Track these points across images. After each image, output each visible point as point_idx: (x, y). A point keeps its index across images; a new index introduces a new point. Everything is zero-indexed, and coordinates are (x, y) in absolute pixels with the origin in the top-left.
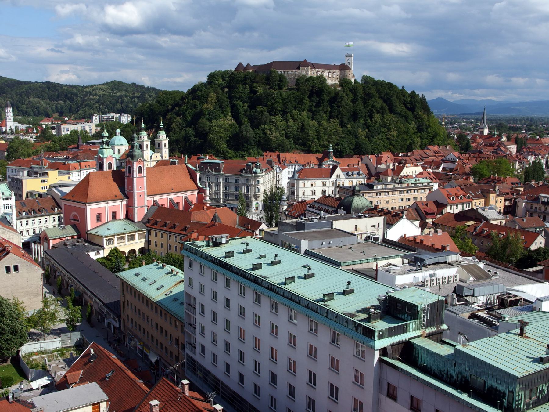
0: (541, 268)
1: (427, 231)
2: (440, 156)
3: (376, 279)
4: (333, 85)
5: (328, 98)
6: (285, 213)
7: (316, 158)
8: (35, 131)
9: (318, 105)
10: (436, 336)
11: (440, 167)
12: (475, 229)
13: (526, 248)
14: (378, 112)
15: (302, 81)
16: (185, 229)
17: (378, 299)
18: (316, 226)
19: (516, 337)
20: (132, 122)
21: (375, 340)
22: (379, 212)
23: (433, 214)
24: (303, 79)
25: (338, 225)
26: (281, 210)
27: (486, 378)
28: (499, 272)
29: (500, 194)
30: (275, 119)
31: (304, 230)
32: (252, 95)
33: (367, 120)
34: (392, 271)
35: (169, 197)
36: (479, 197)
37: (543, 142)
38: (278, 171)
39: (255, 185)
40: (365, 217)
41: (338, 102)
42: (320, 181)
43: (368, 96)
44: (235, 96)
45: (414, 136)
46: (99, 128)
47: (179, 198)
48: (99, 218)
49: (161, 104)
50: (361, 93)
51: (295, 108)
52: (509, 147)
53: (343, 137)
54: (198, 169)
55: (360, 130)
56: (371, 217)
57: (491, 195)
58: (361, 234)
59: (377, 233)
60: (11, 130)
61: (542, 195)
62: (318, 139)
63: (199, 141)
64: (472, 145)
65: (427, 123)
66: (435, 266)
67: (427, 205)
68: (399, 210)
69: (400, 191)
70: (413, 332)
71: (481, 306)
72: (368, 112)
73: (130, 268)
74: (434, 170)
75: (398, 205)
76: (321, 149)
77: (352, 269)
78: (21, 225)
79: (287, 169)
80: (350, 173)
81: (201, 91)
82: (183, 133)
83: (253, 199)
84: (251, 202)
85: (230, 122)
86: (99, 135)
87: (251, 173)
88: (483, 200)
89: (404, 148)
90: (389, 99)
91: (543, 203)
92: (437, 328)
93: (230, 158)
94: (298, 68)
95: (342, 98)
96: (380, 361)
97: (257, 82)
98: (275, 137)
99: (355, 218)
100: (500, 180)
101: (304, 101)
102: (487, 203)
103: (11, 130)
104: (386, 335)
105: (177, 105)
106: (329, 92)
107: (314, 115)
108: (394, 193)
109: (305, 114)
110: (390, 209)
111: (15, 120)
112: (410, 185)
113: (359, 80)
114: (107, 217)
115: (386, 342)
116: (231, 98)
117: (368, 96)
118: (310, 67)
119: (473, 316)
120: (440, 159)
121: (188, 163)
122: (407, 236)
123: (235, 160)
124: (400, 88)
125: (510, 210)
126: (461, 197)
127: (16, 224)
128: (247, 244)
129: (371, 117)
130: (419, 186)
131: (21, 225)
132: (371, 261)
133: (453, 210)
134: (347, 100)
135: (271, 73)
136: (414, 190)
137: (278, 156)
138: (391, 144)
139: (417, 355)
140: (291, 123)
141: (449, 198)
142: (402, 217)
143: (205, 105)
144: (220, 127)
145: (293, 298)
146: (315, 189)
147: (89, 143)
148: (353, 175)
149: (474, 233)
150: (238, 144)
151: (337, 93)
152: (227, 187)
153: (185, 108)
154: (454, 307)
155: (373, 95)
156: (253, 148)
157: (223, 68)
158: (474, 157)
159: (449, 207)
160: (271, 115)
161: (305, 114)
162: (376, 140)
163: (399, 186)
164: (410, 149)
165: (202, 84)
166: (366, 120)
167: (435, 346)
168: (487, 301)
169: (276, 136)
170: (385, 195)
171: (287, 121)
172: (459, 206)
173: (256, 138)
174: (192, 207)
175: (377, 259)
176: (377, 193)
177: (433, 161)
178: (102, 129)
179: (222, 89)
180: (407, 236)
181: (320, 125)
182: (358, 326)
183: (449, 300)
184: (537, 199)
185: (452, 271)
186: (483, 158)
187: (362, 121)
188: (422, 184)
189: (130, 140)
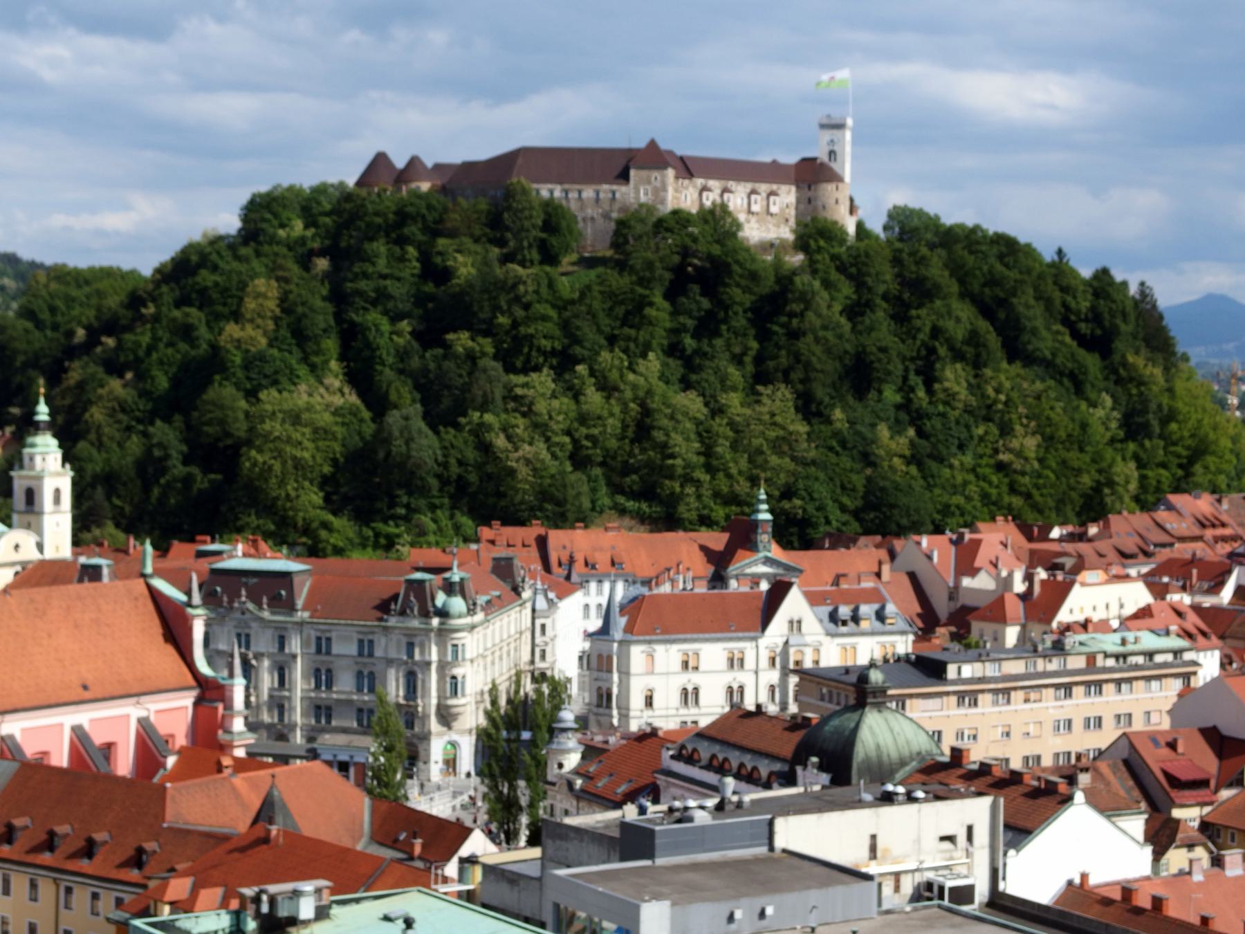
1: (1176, 858)
2: (1224, 539)
5: (748, 300)
6: (570, 785)
7: (704, 549)
9: (707, 327)
15: (639, 228)
16: (138, 859)
18: (703, 838)
23: (1202, 784)
24: (642, 221)
25: (795, 833)
26: (552, 772)
30: (526, 385)
32: (429, 288)
33: (912, 390)
38: (541, 603)
39: (443, 666)
40: (910, 799)
41: (792, 315)
43: (914, 291)
44: (360, 293)
45: (1109, 453)
47: (116, 723)
49: (39, 325)
50: (885, 278)
51: (612, 340)
53: (814, 463)
54: (197, 598)
55: (883, 431)
56: (938, 798)
58: (897, 875)
59: (964, 870)
62: (709, 468)
63: (202, 481)
65: (1165, 400)
67: (1172, 745)
69: (1057, 687)
72: (919, 357)
76: (720, 513)
80: (845, 611)
81: (215, 268)
82: (135, 445)
83: (434, 725)
84: (426, 737)
85: (338, 401)
87: (425, 615)
89: (1069, 507)
90: (1003, 303)
93: (338, 551)
94: (624, 177)
95: (806, 300)
97: (452, 234)
98: (528, 462)
105: (111, 326)
106: (754, 276)
107: (689, 369)
108: (1033, 696)
110: (1016, 765)
112: (1100, 661)
113: (876, 225)
116: (339, 298)
118: (670, 173)
121: (158, 573)
122: (1093, 881)
123: (356, 555)
124: (1048, 255)
129: (930, 380)
130: (1137, 667)
134: (829, 306)
135: (509, 194)
136: (1118, 682)
137: (542, 542)
138: (1013, 490)
140: (594, 398)
142: (1067, 800)
143: (232, 330)
144: (295, 418)
148: (856, 619)
150: (370, 491)
151: (785, 280)
152: (322, 676)
153: (146, 339)
155: (937, 287)
156: (433, 508)
157: (307, 176)
160: (510, 369)
164: (1093, 508)
165: (216, 241)
169: (527, 456)
170: (996, 703)
171: (576, 395)
173: (445, 465)
174: (171, 761)
177: (1194, 561)
179: (305, 261)
180: (1093, 881)
181: (717, 411)
188: (1150, 655)
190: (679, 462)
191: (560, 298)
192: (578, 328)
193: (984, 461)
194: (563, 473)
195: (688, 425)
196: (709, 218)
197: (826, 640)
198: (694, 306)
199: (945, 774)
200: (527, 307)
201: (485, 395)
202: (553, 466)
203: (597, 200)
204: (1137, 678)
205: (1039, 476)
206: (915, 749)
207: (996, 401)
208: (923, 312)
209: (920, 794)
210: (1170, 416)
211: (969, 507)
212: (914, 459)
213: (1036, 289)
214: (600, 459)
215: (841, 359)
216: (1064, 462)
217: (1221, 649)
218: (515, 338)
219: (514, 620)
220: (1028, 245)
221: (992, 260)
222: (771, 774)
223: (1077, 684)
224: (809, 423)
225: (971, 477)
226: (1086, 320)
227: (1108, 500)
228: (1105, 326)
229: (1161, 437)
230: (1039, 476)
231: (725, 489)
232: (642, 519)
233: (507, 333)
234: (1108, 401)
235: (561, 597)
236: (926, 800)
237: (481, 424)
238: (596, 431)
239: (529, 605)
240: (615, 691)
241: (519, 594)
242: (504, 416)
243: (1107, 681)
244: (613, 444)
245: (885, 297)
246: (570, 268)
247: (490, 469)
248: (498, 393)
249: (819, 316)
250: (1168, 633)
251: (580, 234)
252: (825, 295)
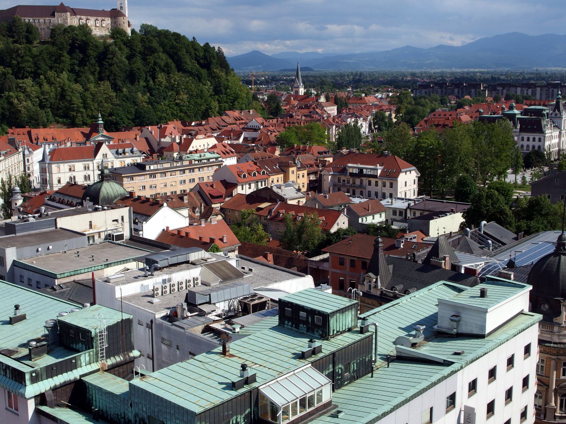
0: (326, 256)
2: (242, 124)
4: (102, 37)
5: (95, 54)
6: (19, 210)
7: (82, 132)
9: (82, 63)
10: (125, 366)
11: (240, 137)
12: (270, 212)
13: (326, 231)
14: (163, 71)
15: (59, 32)
17: (45, 327)
18: (32, 226)
19: (217, 357)
21: (26, 386)
22: (136, 200)
23: (221, 197)
24: (60, 29)
25: (64, 223)
26: (14, 206)
27: (164, 418)
29: (303, 167)
30: (23, 83)
31: (15, 233)
33: (149, 81)
34: (111, 281)
36: (276, 172)
37: (367, 102)
38: (27, 152)
40: (104, 210)
41: (109, 59)
42: (81, 163)
43: (148, 51)
45: (210, 99)
50: (139, 47)
51: (51, 68)
53: (118, 105)
55: (140, 95)
56: (112, 208)
57: (291, 169)
58: (99, 233)
59: (121, 230)
61: (350, 165)
62: (85, 108)
64: (283, 108)
65: (226, 83)
67: (212, 186)
69: (180, 170)
70: (88, 367)
71: (219, 316)
72: (150, 71)
74: (233, 142)
76: (89, 121)
77: (74, 281)
80: (120, 151)
88: (282, 175)
89: (195, 116)
90: (176, 54)
91: (352, 175)
92: (124, 357)
94: (53, 15)
95: (114, 54)
96: (38, 412)
98: (25, 108)
99: (91, 212)
100: (306, 150)
101: (62, 58)
102: (286, 179)
104: (44, 376)
106: (97, 47)
107: (77, 77)
108: (173, 174)
109: (65, 75)
110: (148, 196)
112: (193, 162)
113: (137, 30)
115: (45, 385)
117: (148, 51)
118: (68, 14)
119: (208, 329)
120: (242, 126)
122: (170, 229)
124: (191, 39)
125: (315, 186)
126: (255, 175)
129: (154, 78)
130: (205, 163)
132: (100, 268)
133: (244, 190)
134: (121, 56)
135: (14, 21)
136: (199, 168)
137: (29, 133)
138: (181, 111)
139: (91, 397)
140: (46, 87)
141: (239, 176)
142: (162, 205)
146: (74, 174)
148: (124, 153)
149: (268, 217)
151: (107, 47)
154: (185, 321)
155: (156, 49)
158: (282, 123)
159: (239, 188)
160: (17, 78)
161: (65, 75)
162: (163, 105)
163: (179, 164)
164: (206, 116)
166: (146, 81)
167: (113, 381)
168: (230, 308)
169: (24, 106)
170: (161, 176)
171: (40, 85)
172: (253, 185)
175: (108, 264)
176: (151, 175)
177: (232, 131)
180: (170, 229)
181: (87, 90)
182: (6, 368)
183: (179, 311)
184: (344, 171)
185: (195, 272)
186: (293, 123)
187: (142, 83)
188: (208, 159)
190: (75, 106)
191: (33, 54)
192: (39, 64)
193: (172, 103)
194: (37, 110)
195: (78, 95)
196: (81, 28)
197: (115, 160)
198: (77, 57)
199: (128, 199)
200: (22, 57)
201: (9, 86)
202: (34, 109)
203: (45, 22)
204: (205, 167)
205: (189, 107)
206: (120, 193)
207: (174, 84)
208: (151, 57)
209: (106, 208)
210: (227, 88)
211: (168, 117)
212: (150, 103)
213: (187, 50)
214: (49, 106)
215: (125, 72)
216: (196, 102)
217: (237, 156)
218: (19, 68)
219: (17, 158)
220: (184, 36)
221: (173, 41)
222: (77, 203)
223: (186, 169)
224: (116, 93)
225: (168, 108)
226: (202, 59)
227: (210, 113)
228: (207, 60)
229: (225, 94)
230: (189, 107)
231: (90, 114)
232: (64, 124)
233: (16, 66)
234: (209, 84)
235: (34, 150)
236: (108, 210)
237: (9, 96)
238: (47, 97)
239: (22, 153)
240: (48, 179)
241: (18, 150)
242: (16, 93)
243: (195, 168)
244: (53, 101)
245: (140, 53)
246: (37, 45)
247: (12, 110)
248: (14, 86)
249: (118, 59)
250: (214, 153)
251: (39, 34)
252: (120, 52)
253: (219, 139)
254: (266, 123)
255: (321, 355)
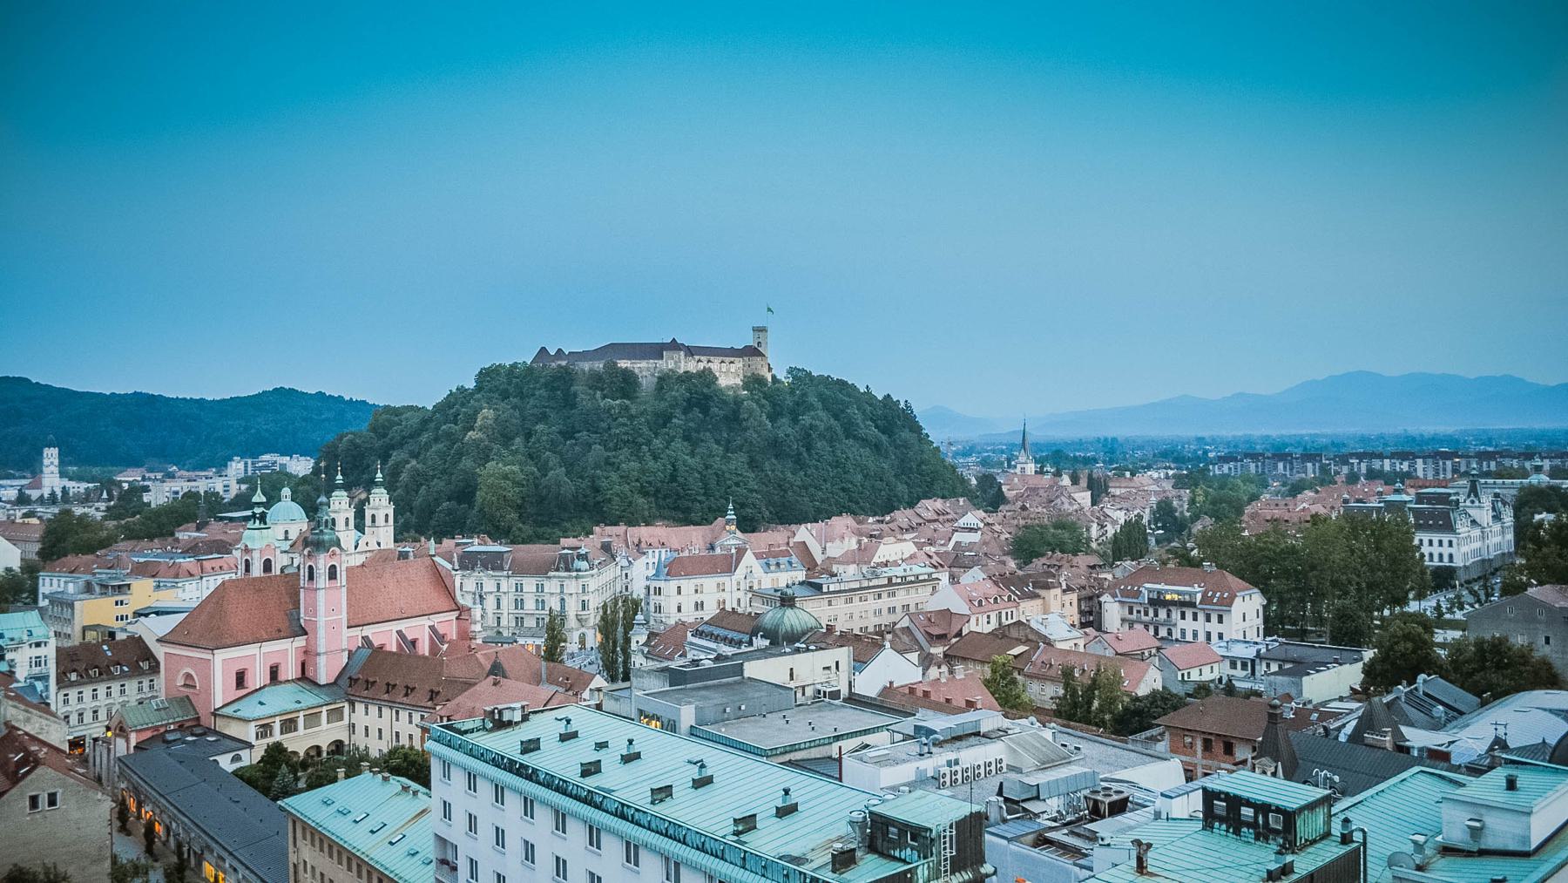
3: (840, 779)
4: (729, 388)
8: (105, 495)
20: (316, 471)
28: (1082, 745)
35: (395, 627)
40: (808, 650)
43: (801, 406)
46: (244, 487)
48: (240, 679)
52: (1076, 496)
60: (53, 494)
66: (958, 744)
68: (876, 633)
71: (1054, 820)
73: (311, 786)
75: (871, 623)
78: (66, 702)
79: (643, 559)
86: (243, 501)
103: (53, 494)
106: (725, 402)
111: (62, 474)
114: (258, 677)
127: (54, 697)
128: (568, 721)
131: (66, 702)
145: (671, 831)
147: (222, 519)
151: (738, 402)
164: (889, 508)
178: (253, 490)
189: (312, 509)
199: (823, 638)
219: (611, 572)
253: (920, 546)
254: (990, 520)
255: (1295, 877)
